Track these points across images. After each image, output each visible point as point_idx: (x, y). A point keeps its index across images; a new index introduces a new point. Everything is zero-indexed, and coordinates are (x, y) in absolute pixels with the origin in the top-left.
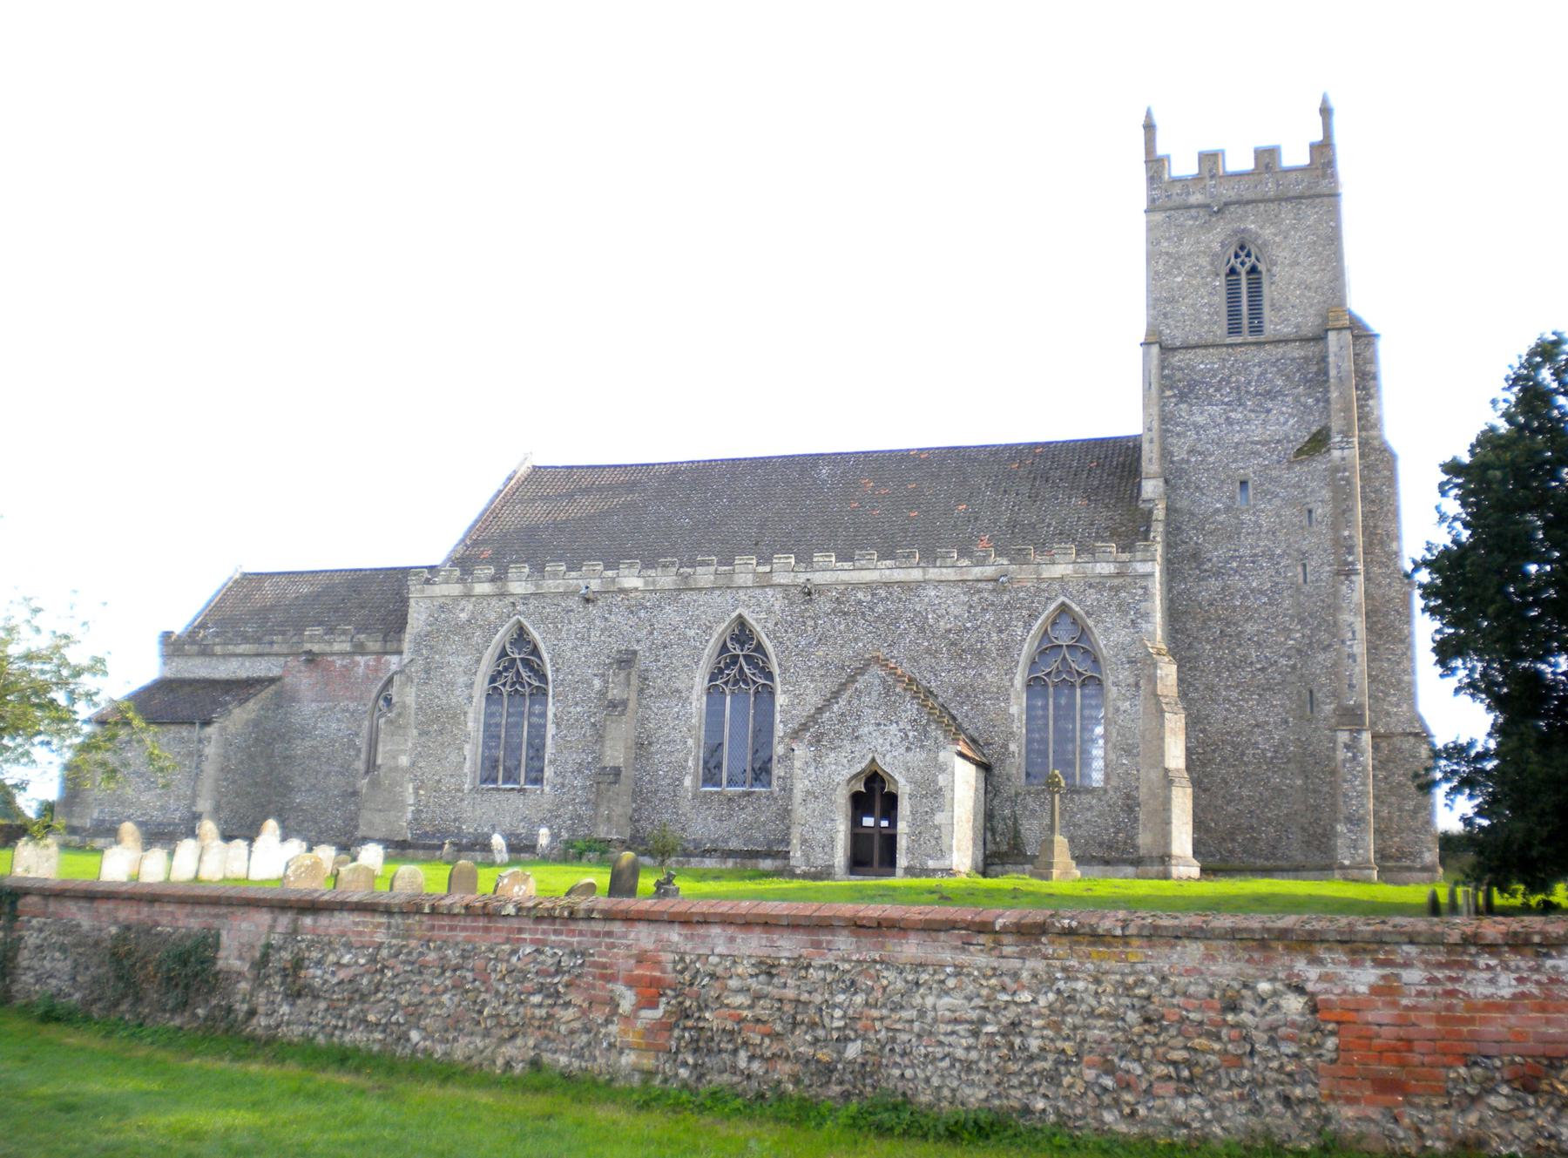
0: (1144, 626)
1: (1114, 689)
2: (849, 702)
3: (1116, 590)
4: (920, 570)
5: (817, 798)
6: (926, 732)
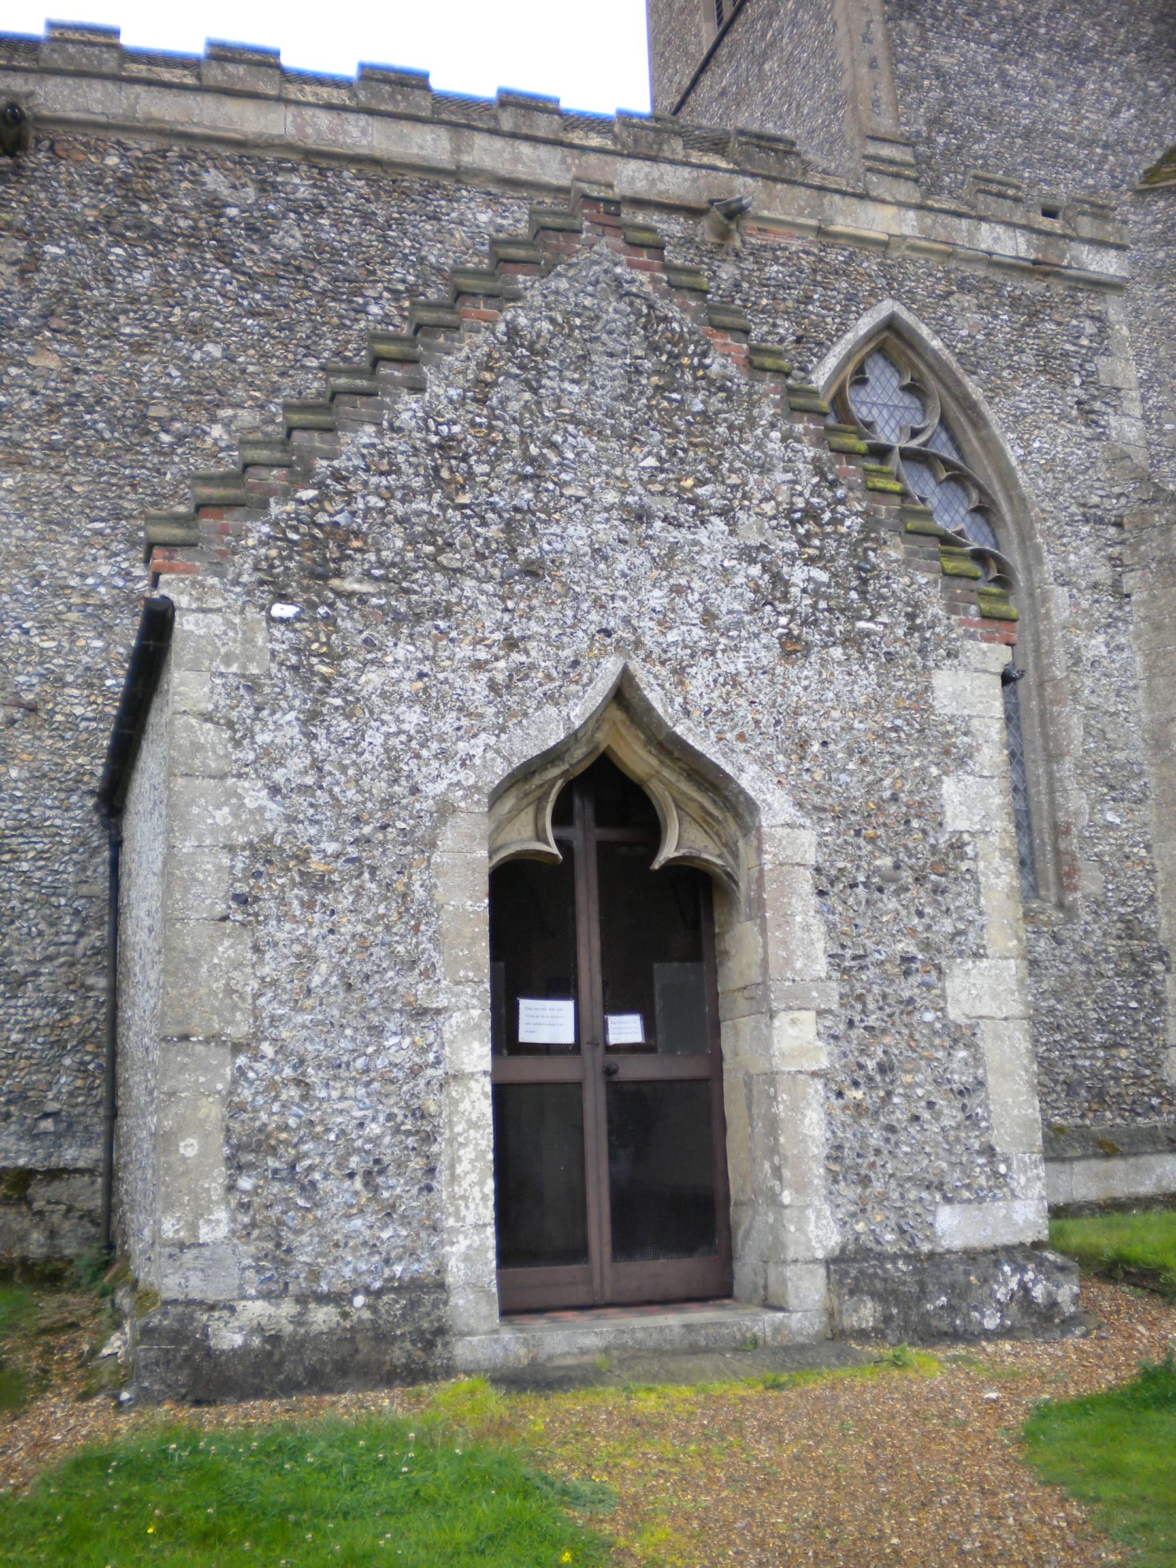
0: (1113, 421)
1: (1061, 594)
2: (481, 391)
3: (1033, 311)
4: (443, 133)
5: (320, 884)
6: (865, 574)
